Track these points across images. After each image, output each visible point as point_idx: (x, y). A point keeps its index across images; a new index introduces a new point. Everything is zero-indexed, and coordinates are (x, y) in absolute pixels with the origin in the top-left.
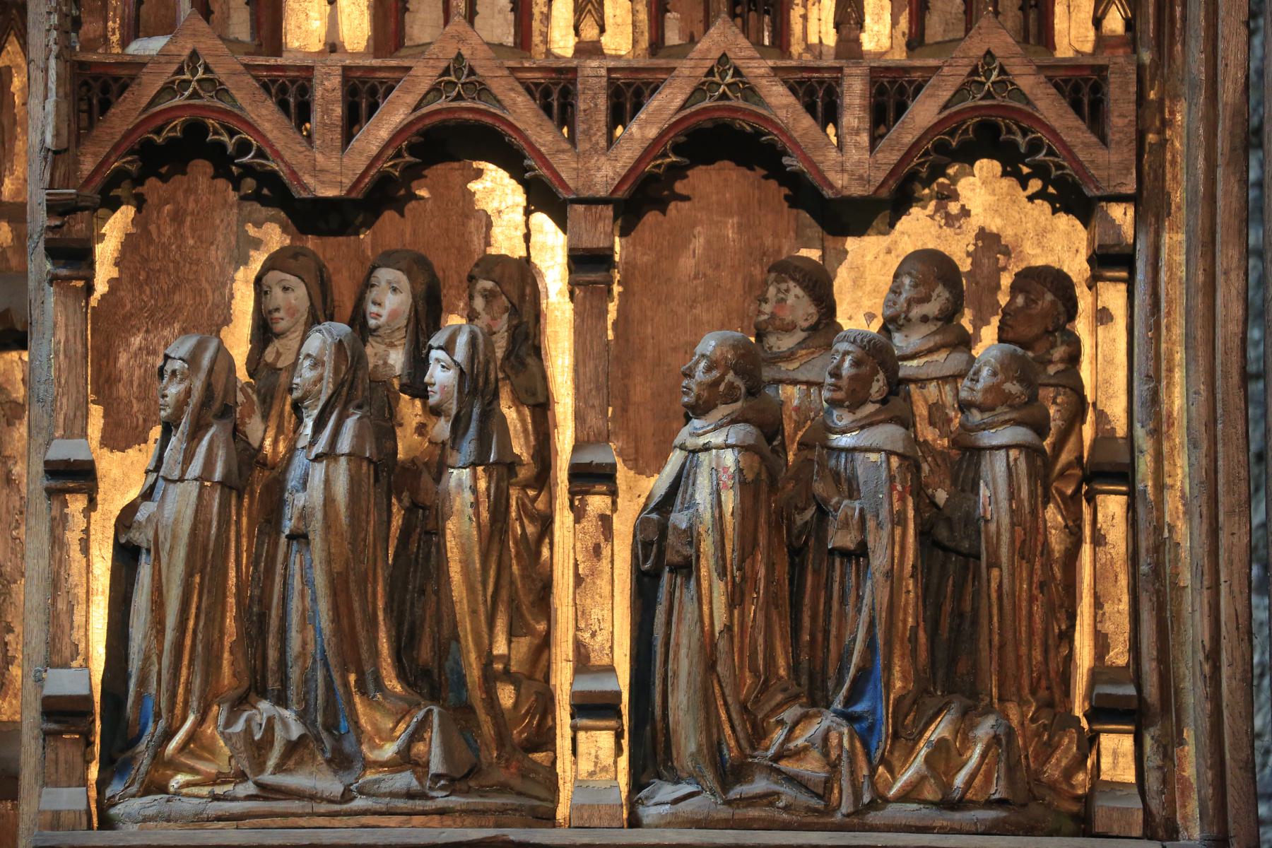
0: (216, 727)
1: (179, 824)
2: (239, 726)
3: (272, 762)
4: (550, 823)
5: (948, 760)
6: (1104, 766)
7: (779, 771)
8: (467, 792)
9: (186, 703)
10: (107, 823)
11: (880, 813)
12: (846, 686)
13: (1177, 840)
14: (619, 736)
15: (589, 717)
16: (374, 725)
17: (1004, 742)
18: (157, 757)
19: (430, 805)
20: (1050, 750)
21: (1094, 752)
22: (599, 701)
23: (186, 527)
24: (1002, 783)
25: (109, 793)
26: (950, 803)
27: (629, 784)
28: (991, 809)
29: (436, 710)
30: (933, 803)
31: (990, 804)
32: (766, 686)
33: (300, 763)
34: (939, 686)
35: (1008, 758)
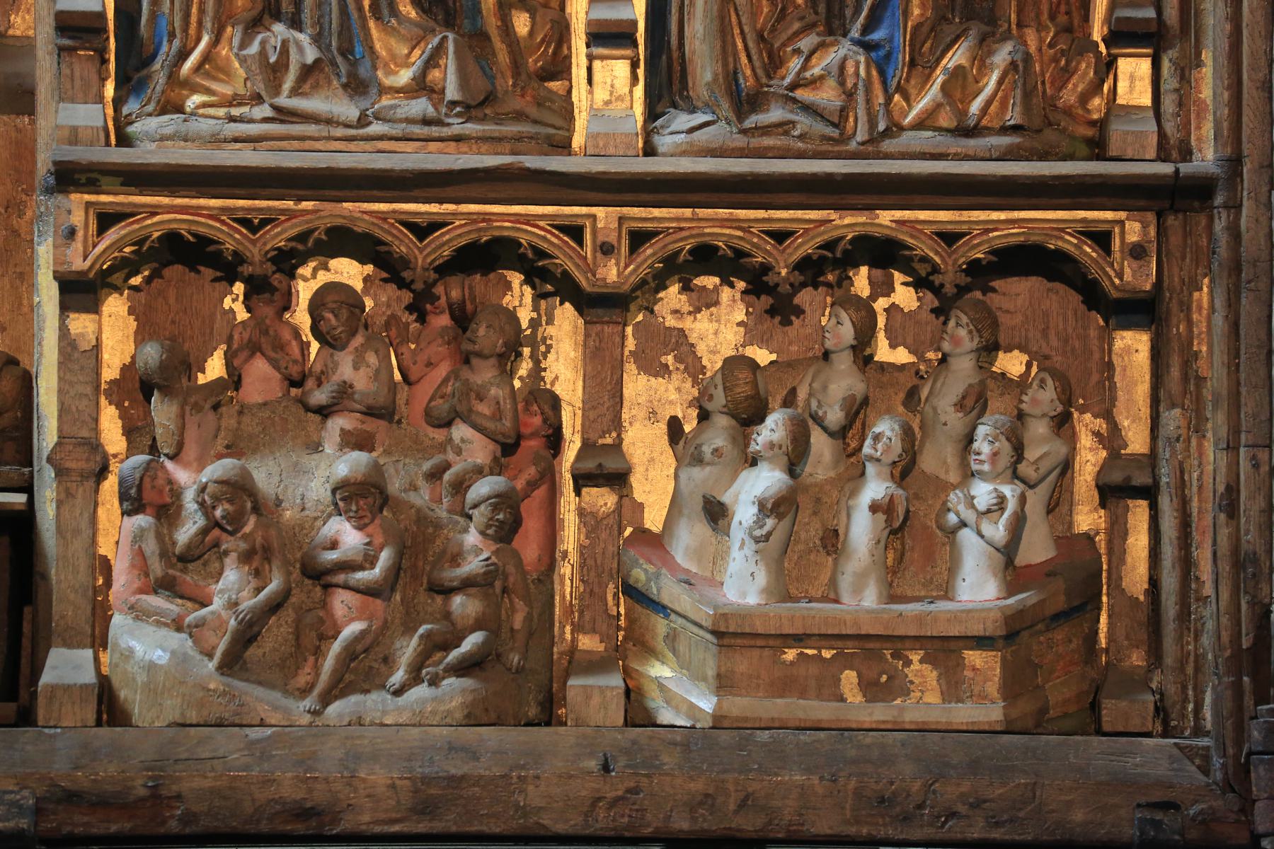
0: (231, 49)
1: (196, 144)
2: (254, 48)
3: (287, 85)
4: (566, 151)
5: (964, 87)
6: (1120, 90)
7: (794, 100)
8: (483, 119)
9: (200, 23)
10: (124, 140)
11: (894, 141)
12: (864, 14)
13: (1191, 161)
14: (634, 65)
15: (604, 45)
16: (390, 51)
17: (1021, 68)
18: (173, 77)
19: (446, 131)
20: (1067, 75)
21: (1111, 76)
22: (614, 30)
24: (1017, 109)
25: (125, 111)
26: (966, 131)
27: (644, 113)
28: (1005, 135)
29: (451, 36)
30: (947, 130)
31: (1005, 130)
32: (783, 15)
33: (316, 87)
34: (957, 13)
35: (1024, 84)
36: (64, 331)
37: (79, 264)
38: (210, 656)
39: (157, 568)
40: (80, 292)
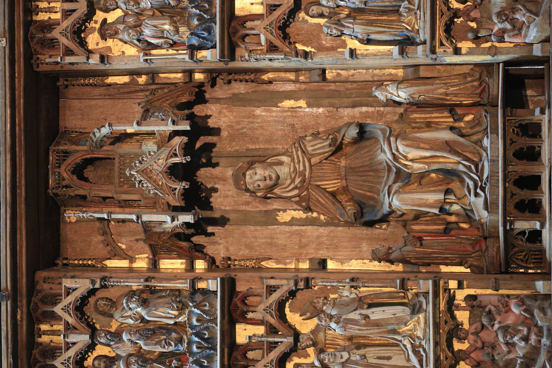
2: (405, 14)
9: (400, 26)
18: (411, 31)
23: (363, 27)
36: (466, 54)
37: (451, 50)
38: (535, 19)
39: (516, 32)
40: (457, 51)
